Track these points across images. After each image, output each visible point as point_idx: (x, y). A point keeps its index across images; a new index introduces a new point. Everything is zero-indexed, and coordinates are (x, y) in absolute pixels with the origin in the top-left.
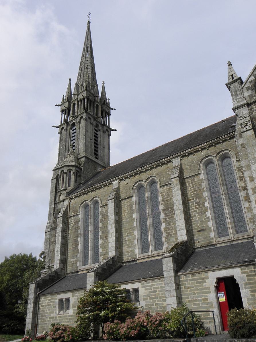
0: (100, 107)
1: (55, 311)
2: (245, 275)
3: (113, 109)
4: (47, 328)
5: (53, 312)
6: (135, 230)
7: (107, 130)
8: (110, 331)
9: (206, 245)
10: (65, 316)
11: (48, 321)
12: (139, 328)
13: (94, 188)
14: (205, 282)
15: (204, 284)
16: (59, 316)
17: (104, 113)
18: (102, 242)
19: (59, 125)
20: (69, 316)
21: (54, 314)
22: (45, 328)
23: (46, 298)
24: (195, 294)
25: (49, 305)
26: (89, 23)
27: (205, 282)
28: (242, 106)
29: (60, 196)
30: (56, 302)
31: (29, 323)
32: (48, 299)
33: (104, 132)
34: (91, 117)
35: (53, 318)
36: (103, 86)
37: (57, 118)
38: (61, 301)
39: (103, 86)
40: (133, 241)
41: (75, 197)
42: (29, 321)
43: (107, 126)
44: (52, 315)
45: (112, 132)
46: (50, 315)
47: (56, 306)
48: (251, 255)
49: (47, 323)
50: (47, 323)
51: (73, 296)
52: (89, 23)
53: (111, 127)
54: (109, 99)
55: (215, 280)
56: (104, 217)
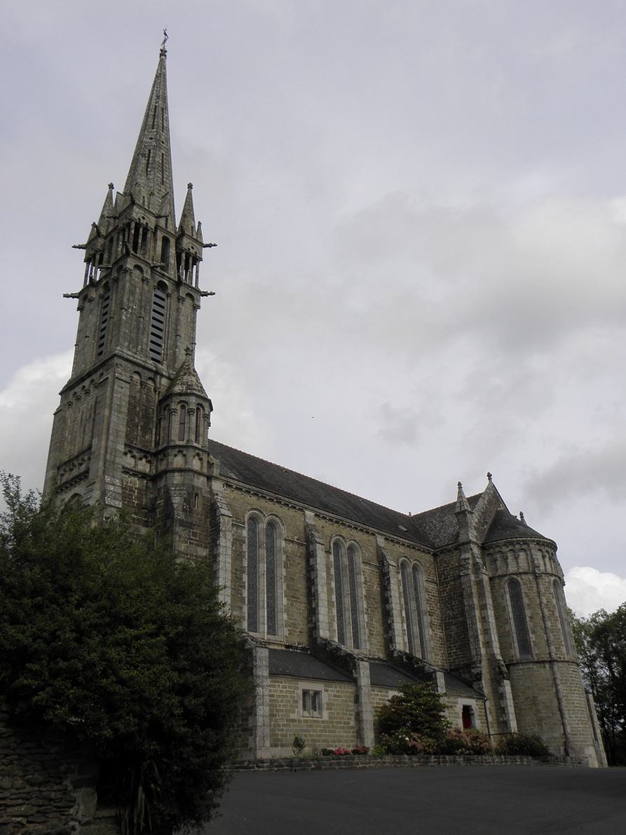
1: (296, 710)
7: (189, 295)
9: (549, 624)
10: (314, 721)
11: (284, 725)
17: (183, 256)
20: (323, 722)
21: (296, 714)
22: (280, 737)
23: (278, 682)
24: (574, 703)
26: (163, 53)
32: (281, 685)
33: (180, 299)
35: (294, 720)
36: (189, 194)
38: (305, 693)
39: (189, 194)
41: (237, 488)
44: (292, 716)
48: (20, 636)
51: (326, 691)
52: (163, 53)
53: (202, 288)
55: (462, 707)
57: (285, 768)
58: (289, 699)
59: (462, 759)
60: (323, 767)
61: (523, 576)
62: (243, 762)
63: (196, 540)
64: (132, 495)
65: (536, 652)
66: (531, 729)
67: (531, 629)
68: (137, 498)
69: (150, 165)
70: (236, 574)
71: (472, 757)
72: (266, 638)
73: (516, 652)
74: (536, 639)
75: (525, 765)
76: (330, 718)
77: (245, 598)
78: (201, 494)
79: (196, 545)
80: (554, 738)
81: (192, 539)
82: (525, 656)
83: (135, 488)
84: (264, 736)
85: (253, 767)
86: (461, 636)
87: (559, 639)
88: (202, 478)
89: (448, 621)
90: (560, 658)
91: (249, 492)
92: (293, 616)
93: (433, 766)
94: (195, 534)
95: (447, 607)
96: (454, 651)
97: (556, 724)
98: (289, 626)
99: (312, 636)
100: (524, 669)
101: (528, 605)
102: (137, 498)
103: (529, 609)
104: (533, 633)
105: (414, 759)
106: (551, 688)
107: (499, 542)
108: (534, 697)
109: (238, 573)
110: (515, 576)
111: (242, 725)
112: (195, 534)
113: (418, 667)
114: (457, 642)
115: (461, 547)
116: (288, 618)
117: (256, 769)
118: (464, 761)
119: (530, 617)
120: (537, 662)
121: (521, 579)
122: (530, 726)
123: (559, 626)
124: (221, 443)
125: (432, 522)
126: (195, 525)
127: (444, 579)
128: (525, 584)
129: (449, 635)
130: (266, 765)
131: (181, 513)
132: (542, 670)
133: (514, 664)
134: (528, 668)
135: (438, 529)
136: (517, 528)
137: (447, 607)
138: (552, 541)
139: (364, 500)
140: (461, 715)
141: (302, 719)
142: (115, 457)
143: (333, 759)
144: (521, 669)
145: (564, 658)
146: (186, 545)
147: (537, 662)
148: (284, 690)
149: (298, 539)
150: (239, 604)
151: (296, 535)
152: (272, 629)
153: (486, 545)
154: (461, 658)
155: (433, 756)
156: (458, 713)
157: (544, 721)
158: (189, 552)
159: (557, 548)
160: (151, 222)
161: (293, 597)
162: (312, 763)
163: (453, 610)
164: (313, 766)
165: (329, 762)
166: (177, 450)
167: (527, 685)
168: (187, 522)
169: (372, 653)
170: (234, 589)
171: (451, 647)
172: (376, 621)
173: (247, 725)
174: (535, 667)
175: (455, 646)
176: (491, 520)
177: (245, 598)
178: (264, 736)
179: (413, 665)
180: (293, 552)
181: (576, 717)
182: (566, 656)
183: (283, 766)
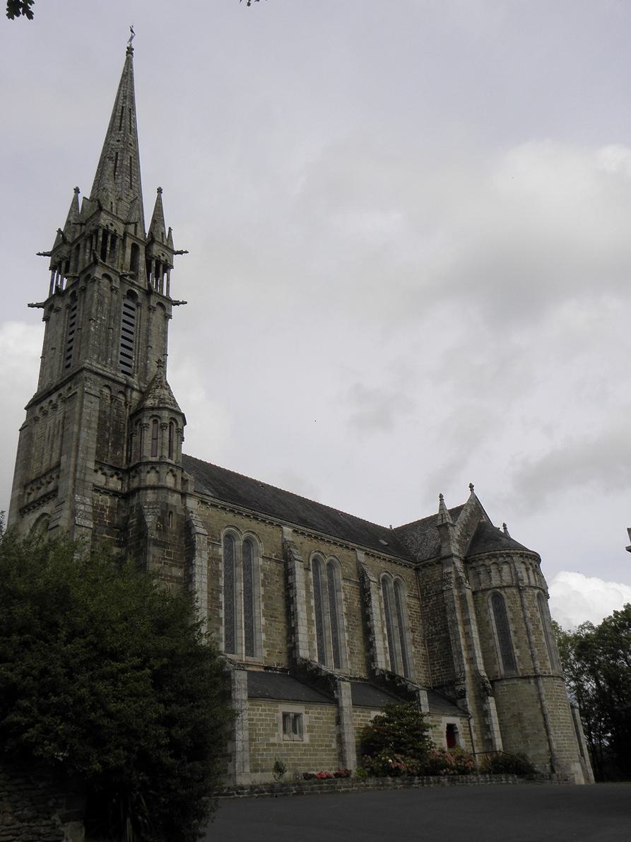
0: (142, 248)
1: (276, 734)
3: (181, 254)
4: (264, 763)
5: (273, 735)
6: (313, 625)
7: (160, 304)
10: (295, 744)
11: (264, 750)
12: (50, 697)
17: (154, 263)
18: (266, 624)
19: (43, 301)
20: (304, 745)
21: (276, 738)
22: (260, 762)
25: (263, 720)
26: (130, 51)
30: (278, 718)
34: (111, 275)
35: (274, 745)
37: (40, 281)
38: (285, 716)
42: (243, 746)
43: (160, 295)
44: (272, 740)
45: (174, 308)
46: (269, 740)
47: (277, 724)
49: (263, 754)
50: (263, 754)
53: (173, 297)
54: (170, 228)
55: (446, 726)
62: (223, 789)
63: (170, 560)
66: (516, 747)
68: (108, 517)
70: (211, 594)
72: (244, 659)
73: (500, 668)
76: (311, 741)
81: (166, 559)
83: (107, 507)
85: (233, 794)
90: (545, 673)
91: (234, 511)
96: (438, 667)
102: (108, 517)
103: (513, 622)
106: (535, 704)
110: (498, 590)
116: (267, 639)
117: (236, 795)
120: (521, 678)
121: (505, 592)
123: (544, 640)
125: (413, 536)
127: (426, 594)
128: (508, 598)
130: (246, 791)
132: (527, 686)
133: (498, 680)
134: (512, 684)
140: (445, 734)
142: (85, 474)
143: (315, 783)
149: (275, 557)
152: (250, 650)
154: (445, 675)
159: (540, 560)
160: (120, 229)
161: (272, 617)
164: (295, 792)
174: (520, 683)
183: (263, 792)
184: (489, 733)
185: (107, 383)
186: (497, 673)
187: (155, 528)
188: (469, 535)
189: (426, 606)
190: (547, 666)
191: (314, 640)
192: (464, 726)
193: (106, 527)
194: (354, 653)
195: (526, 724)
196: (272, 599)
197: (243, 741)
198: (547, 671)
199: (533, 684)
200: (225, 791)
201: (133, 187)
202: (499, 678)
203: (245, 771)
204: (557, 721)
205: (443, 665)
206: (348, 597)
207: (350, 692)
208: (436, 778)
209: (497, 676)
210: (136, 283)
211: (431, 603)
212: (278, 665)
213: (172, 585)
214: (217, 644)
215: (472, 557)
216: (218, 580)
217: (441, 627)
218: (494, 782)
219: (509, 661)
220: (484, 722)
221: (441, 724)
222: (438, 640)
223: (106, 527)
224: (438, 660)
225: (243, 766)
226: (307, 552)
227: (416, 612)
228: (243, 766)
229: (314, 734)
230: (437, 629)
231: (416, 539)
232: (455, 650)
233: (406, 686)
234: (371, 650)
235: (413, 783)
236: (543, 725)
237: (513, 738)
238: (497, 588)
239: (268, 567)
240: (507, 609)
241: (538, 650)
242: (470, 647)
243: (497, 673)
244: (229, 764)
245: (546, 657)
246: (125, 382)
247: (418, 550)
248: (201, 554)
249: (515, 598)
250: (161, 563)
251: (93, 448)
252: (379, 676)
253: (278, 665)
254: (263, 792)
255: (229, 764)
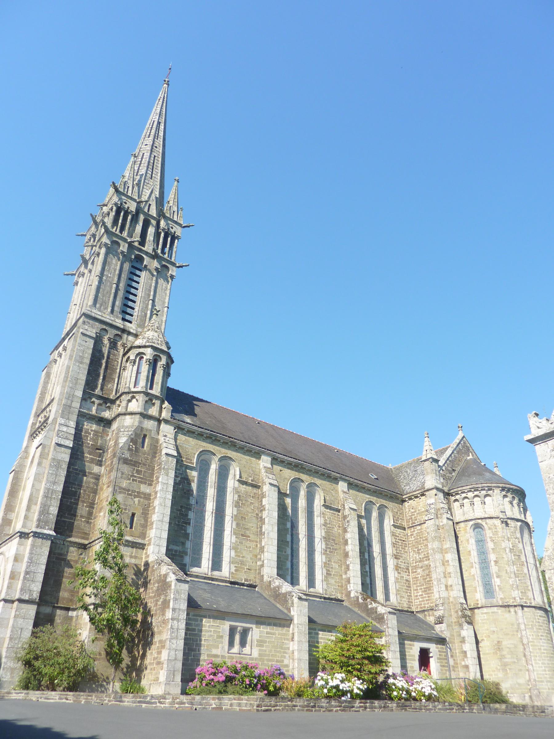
1: (220, 645)
2: (437, 650)
5: (217, 647)
6: (288, 547)
8: (384, 692)
13: (231, 442)
14: (412, 649)
15: (411, 651)
16: (231, 657)
18: (236, 542)
27: (412, 649)
28: (518, 520)
29: (129, 401)
30: (223, 630)
31: (176, 659)
38: (232, 630)
40: (285, 562)
42: (176, 655)
55: (419, 650)
56: (242, 501)
57: (187, 705)
58: (212, 634)
59: (395, 705)
60: (224, 707)
61: (488, 520)
62: (146, 697)
63: (140, 478)
64: (87, 436)
65: (501, 596)
66: (495, 675)
67: (496, 573)
68: (92, 439)
69: (142, 165)
70: (180, 510)
71: (408, 703)
72: (210, 574)
73: (477, 596)
74: (501, 583)
75: (475, 713)
76: (260, 655)
77: (189, 534)
78: (150, 435)
79: (139, 482)
80: (519, 684)
81: (135, 477)
82: (490, 600)
83: (92, 430)
84: (174, 671)
85: (155, 703)
86: (426, 579)
87: (525, 583)
88: (152, 422)
89: (415, 564)
90: (526, 602)
91: (211, 438)
92: (242, 553)
93: (359, 711)
94: (138, 472)
95: (414, 551)
96: (420, 593)
97: (521, 670)
98: (236, 563)
99: (260, 573)
100: (489, 613)
101: (493, 549)
102: (92, 439)
103: (494, 552)
104: (498, 577)
105: (333, 703)
106: (515, 633)
107: (464, 488)
108: (498, 642)
109: (183, 510)
110: (480, 521)
111: (157, 658)
112: (138, 472)
113: (371, 608)
114: (423, 585)
115: (426, 493)
116: (236, 556)
117: (158, 704)
118: (397, 706)
119: (495, 561)
120: (501, 606)
121: (486, 523)
122: (494, 671)
123: (526, 571)
124: (191, 394)
125: (407, 472)
126: (140, 464)
127: (412, 524)
128: (490, 529)
129: (416, 578)
130: (167, 701)
131: (126, 452)
132: (507, 615)
133: (479, 608)
134: (493, 613)
135: (410, 477)
136: (484, 475)
137: (414, 551)
138: (520, 488)
139: (350, 457)
140: (417, 658)
141: (227, 655)
142: (72, 401)
143: (235, 699)
144: (486, 613)
145: (531, 603)
146: (128, 481)
147: (501, 606)
148: (208, 624)
149: (252, 481)
150: (182, 540)
151: (250, 477)
152: (216, 564)
153: (452, 491)
154: (426, 600)
155: (358, 701)
156: (414, 656)
157: (509, 667)
158: (131, 489)
159: (525, 496)
160: (133, 207)
161: (242, 535)
162: (213, 702)
163: (419, 553)
164: (214, 706)
165: (230, 702)
166: (130, 395)
167: (492, 629)
168: (131, 461)
169: (328, 592)
170: (178, 525)
171: (417, 590)
172: (335, 562)
173: (160, 658)
174: (500, 611)
175: (421, 589)
176: (459, 468)
177: (189, 534)
178: (174, 671)
179: (367, 606)
180: (247, 492)
181: (542, 663)
182: (533, 601)
183: (184, 703)
184: (466, 660)
185: (104, 327)
186: (478, 600)
187: (127, 448)
188: (454, 470)
189: (412, 535)
190: (528, 596)
191: (287, 560)
192: (439, 651)
193: (89, 447)
194: (331, 575)
195: (505, 653)
196: (245, 519)
197: (176, 650)
198: (528, 601)
199: (513, 613)
200: (148, 699)
201: (153, 178)
202: (479, 606)
203: (175, 680)
204: (538, 651)
205: (425, 591)
206: (328, 522)
207: (307, 609)
208: (382, 703)
209: (478, 604)
210: (143, 248)
211: (416, 532)
212: (246, 580)
213: (139, 501)
214: (182, 557)
215: (455, 490)
216: (189, 499)
217: (425, 555)
218: (454, 711)
219: (489, 591)
220: (462, 648)
221: (413, 647)
222: (422, 567)
223: (89, 447)
224: (421, 586)
225: (174, 675)
226: (286, 479)
227: (401, 540)
228: (174, 675)
229: (264, 648)
230: (421, 556)
231: (408, 475)
232: (435, 577)
233: (376, 608)
234: (348, 572)
235: (353, 707)
236: (522, 654)
237: (492, 666)
238: (479, 519)
239: (243, 489)
240: (489, 540)
241: (519, 580)
242: (31, 501)
243: (478, 600)
244: (161, 671)
245: (527, 587)
246: (122, 327)
247: (408, 484)
248: (168, 473)
249: (496, 528)
250: (129, 479)
251: (82, 380)
252: (354, 597)
253: (246, 580)
254: (184, 703)
255: (161, 671)
